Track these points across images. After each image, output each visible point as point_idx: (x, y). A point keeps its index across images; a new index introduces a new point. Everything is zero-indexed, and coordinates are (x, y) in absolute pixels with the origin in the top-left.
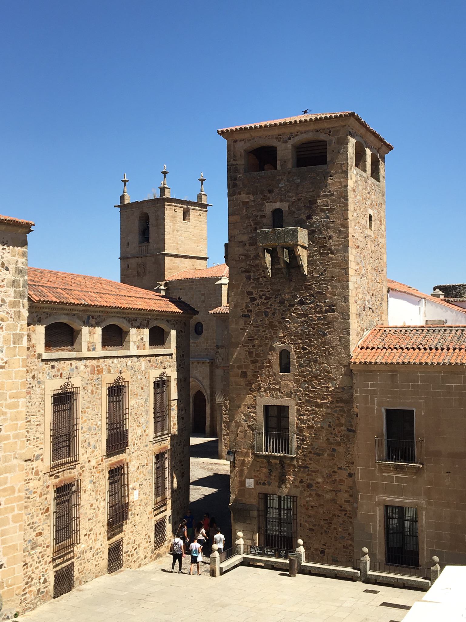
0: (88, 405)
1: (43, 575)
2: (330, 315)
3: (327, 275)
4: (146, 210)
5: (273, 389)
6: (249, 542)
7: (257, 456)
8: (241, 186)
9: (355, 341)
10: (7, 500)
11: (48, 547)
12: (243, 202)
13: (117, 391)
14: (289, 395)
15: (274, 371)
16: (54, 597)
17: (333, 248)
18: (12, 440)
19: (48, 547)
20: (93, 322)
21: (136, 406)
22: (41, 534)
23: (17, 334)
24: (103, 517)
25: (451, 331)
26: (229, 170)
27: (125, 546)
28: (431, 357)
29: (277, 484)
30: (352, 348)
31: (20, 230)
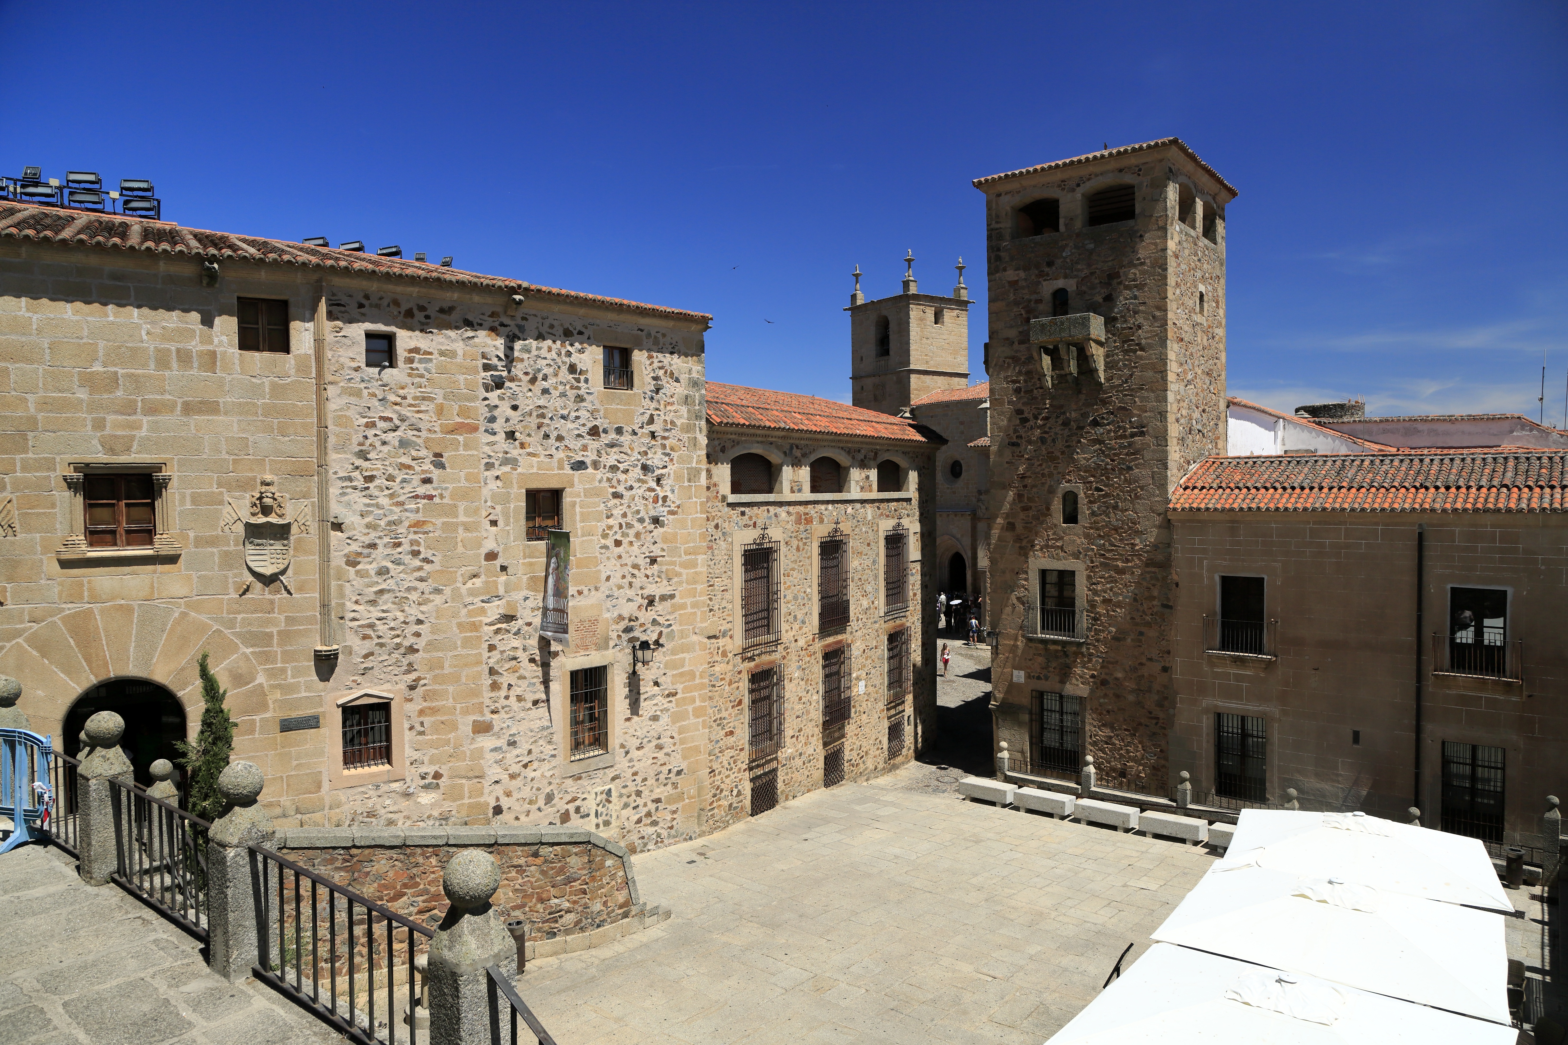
0: (792, 565)
1: (736, 786)
2: (1138, 439)
3: (1134, 382)
4: (885, 313)
5: (1052, 547)
6: (1019, 756)
7: (1030, 640)
8: (1007, 259)
9: (1175, 479)
10: (685, 687)
11: (742, 750)
12: (1009, 282)
13: (832, 549)
14: (1076, 555)
15: (1055, 521)
16: (752, 815)
17: (1143, 342)
18: (689, 610)
19: (742, 750)
20: (797, 453)
21: (860, 568)
22: (731, 733)
23: (692, 468)
24: (817, 714)
25: (1325, 461)
26: (989, 238)
27: (847, 752)
28: (1293, 500)
29: (1057, 678)
30: (1171, 489)
31: (694, 327)
